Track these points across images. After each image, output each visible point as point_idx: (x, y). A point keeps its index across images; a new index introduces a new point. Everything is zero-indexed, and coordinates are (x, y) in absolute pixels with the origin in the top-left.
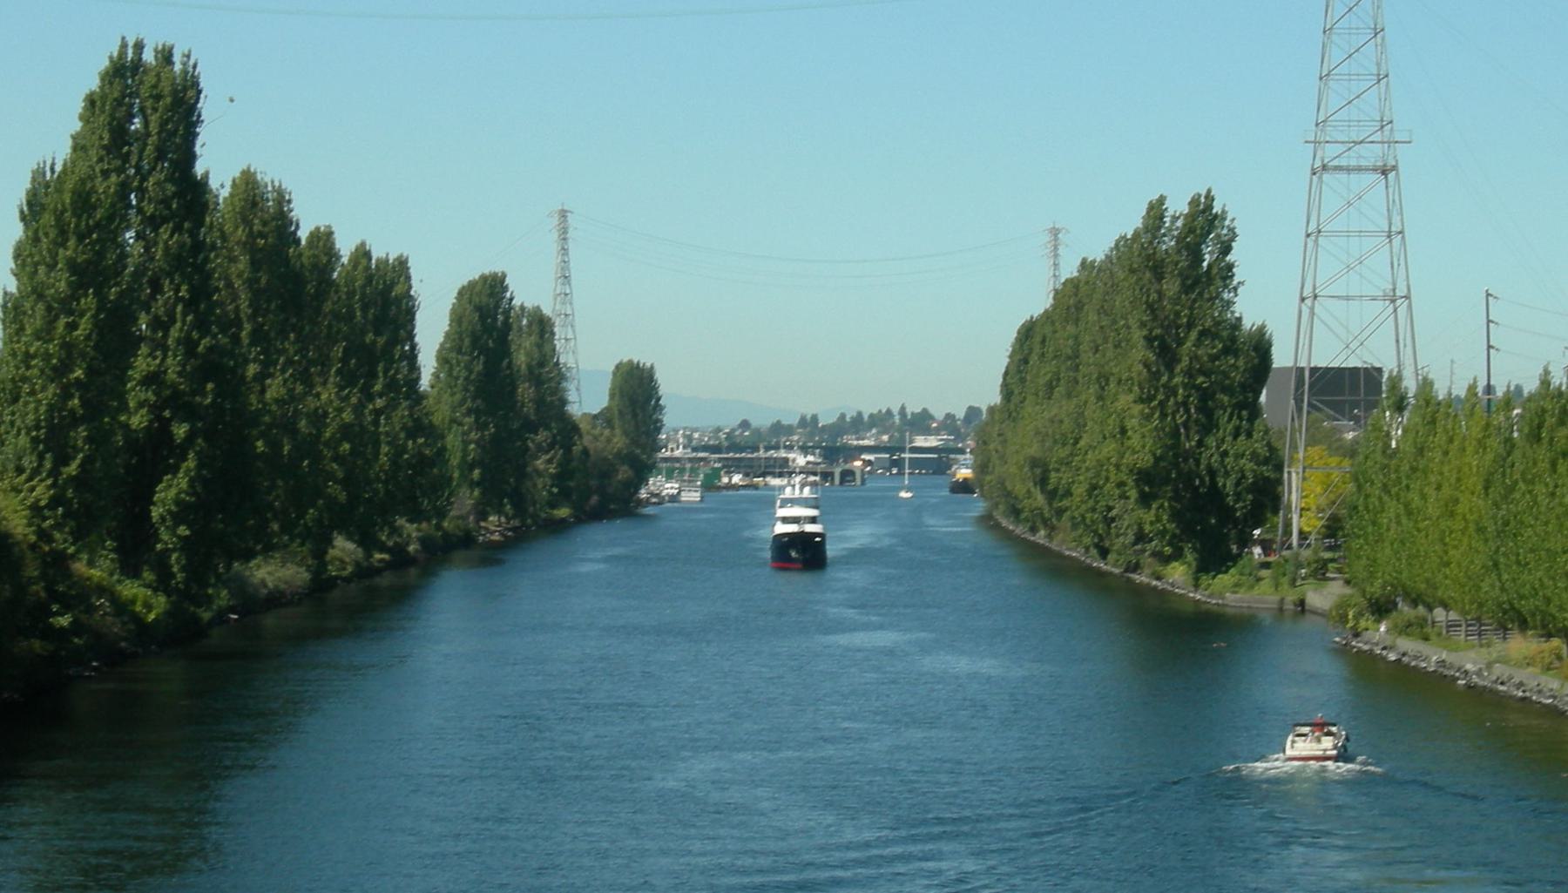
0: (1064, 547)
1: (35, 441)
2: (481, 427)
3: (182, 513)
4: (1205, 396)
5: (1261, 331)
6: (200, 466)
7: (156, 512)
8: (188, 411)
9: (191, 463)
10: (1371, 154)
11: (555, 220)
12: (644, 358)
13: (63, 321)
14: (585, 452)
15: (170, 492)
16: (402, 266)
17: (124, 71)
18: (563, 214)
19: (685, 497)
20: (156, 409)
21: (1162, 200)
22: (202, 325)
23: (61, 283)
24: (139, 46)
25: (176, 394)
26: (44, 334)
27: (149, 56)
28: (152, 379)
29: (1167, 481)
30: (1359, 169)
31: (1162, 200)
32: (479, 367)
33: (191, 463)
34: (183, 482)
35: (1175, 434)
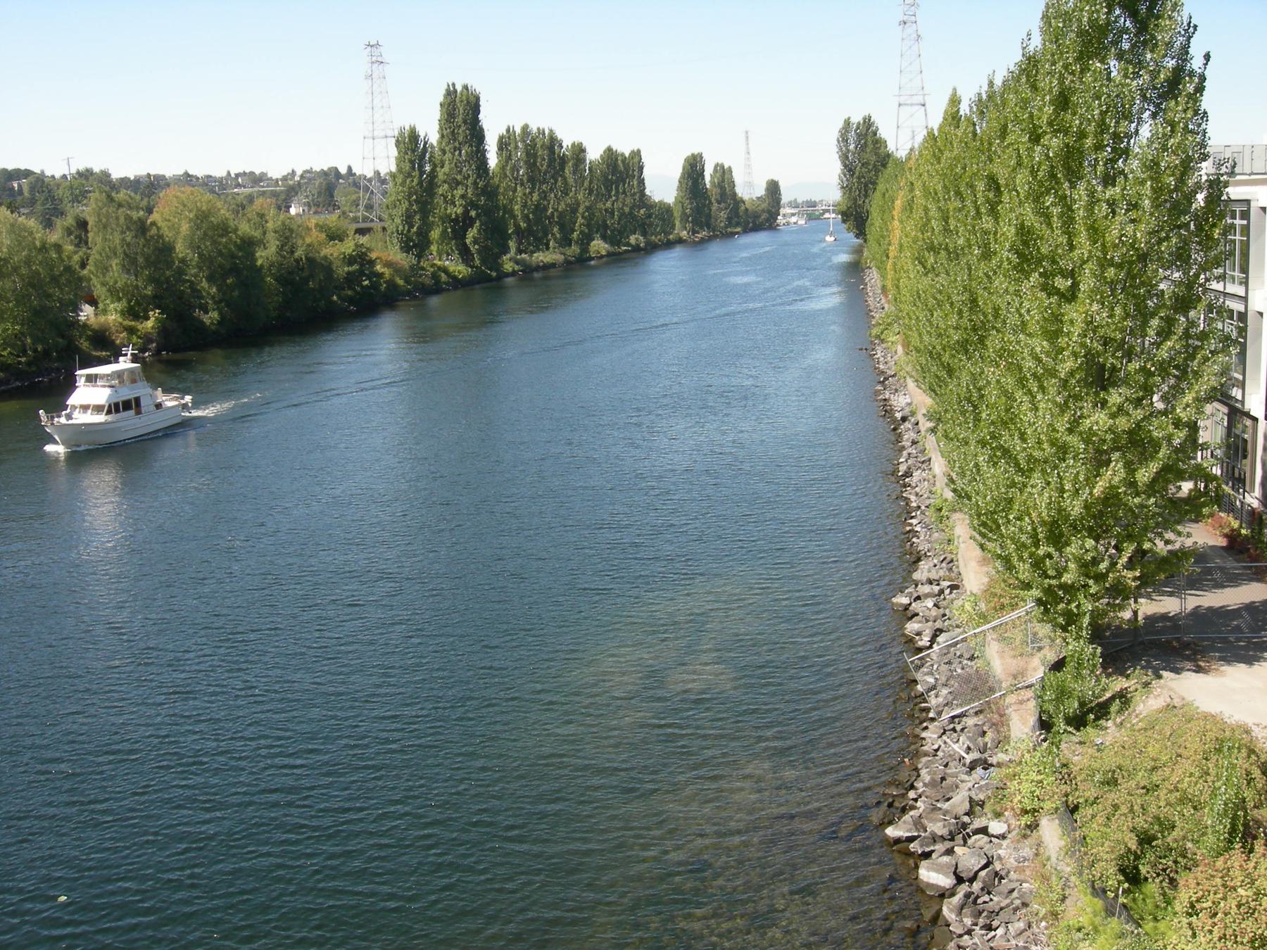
0: (92, 269)
1: (402, 221)
2: (692, 203)
3: (475, 241)
4: (866, 185)
5: (730, 167)
6: (480, 226)
7: (468, 241)
8: (474, 205)
9: (478, 224)
10: (920, 99)
11: (744, 135)
12: (776, 179)
13: (408, 181)
14: (747, 209)
15: (472, 234)
16: (637, 154)
17: (451, 93)
18: (747, 132)
19: (800, 222)
20: (465, 207)
21: (849, 118)
22: (479, 176)
23: (407, 167)
24: (454, 85)
25: (472, 201)
26: (403, 184)
27: (459, 88)
28: (463, 197)
29: (852, 215)
30: (912, 105)
31: (849, 118)
32: (690, 183)
33: (478, 224)
34: (475, 230)
35: (855, 200)
